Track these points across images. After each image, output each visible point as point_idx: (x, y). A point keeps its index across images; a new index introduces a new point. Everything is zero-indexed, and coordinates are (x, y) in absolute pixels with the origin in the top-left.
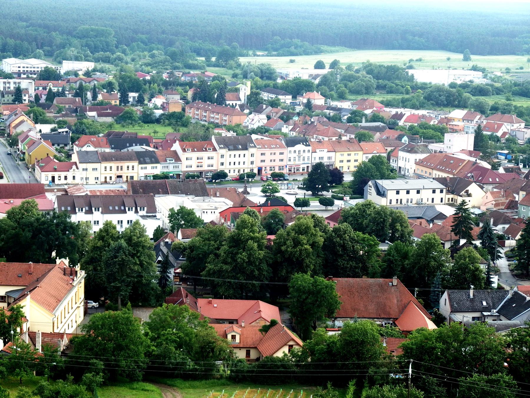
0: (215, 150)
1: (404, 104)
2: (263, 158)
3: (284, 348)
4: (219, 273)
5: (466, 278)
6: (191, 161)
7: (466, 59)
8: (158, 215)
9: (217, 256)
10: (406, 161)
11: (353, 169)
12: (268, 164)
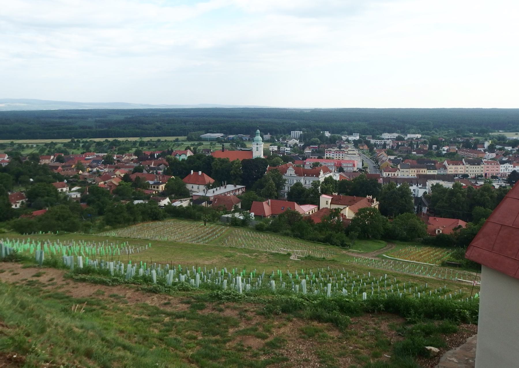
0: (463, 165)
9: (443, 200)
12: (490, 172)
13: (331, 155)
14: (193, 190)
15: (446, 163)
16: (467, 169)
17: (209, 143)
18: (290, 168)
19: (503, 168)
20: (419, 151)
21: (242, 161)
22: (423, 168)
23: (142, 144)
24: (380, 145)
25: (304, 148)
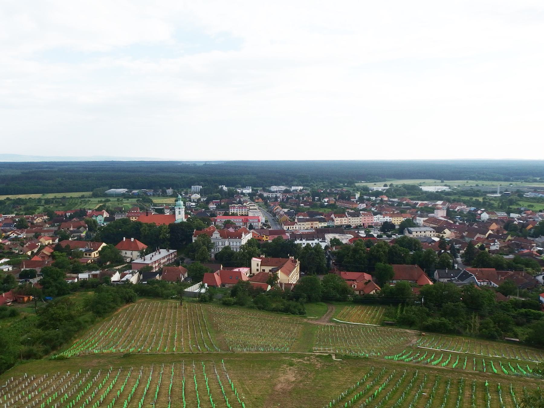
6: (338, 221)
7: (442, 182)
9: (348, 256)
10: (420, 220)
12: (366, 222)
13: (235, 210)
14: (127, 255)
15: (333, 216)
17: (116, 199)
18: (215, 232)
19: (376, 219)
20: (305, 203)
21: (169, 225)
23: (48, 201)
24: (272, 198)
25: (207, 202)
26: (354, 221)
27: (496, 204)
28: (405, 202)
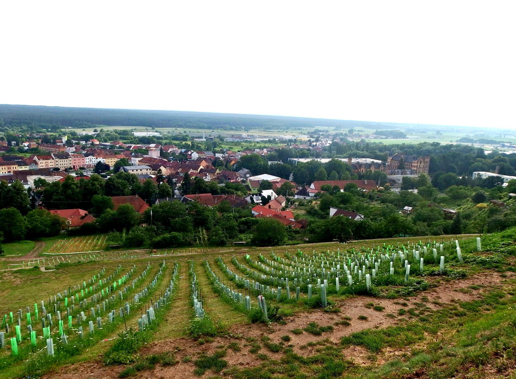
0: (53, 159)
1: (131, 143)
2: (75, 161)
3: (91, 219)
4: (60, 200)
5: (164, 194)
6: (42, 164)
7: (153, 129)
8: (29, 183)
9: (58, 193)
10: (136, 161)
11: (113, 165)
15: (36, 158)
16: (57, 163)
19: (88, 160)
22: (14, 164)
26: (63, 164)
27: (203, 147)
28: (118, 145)
